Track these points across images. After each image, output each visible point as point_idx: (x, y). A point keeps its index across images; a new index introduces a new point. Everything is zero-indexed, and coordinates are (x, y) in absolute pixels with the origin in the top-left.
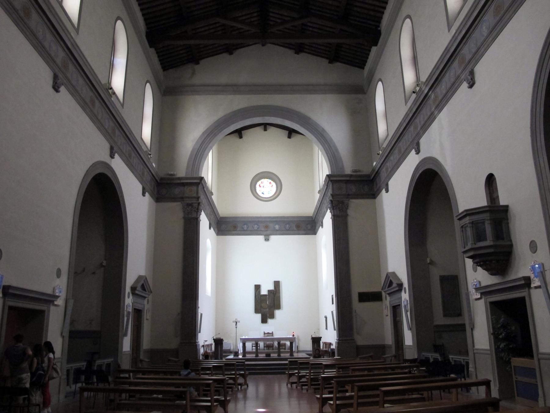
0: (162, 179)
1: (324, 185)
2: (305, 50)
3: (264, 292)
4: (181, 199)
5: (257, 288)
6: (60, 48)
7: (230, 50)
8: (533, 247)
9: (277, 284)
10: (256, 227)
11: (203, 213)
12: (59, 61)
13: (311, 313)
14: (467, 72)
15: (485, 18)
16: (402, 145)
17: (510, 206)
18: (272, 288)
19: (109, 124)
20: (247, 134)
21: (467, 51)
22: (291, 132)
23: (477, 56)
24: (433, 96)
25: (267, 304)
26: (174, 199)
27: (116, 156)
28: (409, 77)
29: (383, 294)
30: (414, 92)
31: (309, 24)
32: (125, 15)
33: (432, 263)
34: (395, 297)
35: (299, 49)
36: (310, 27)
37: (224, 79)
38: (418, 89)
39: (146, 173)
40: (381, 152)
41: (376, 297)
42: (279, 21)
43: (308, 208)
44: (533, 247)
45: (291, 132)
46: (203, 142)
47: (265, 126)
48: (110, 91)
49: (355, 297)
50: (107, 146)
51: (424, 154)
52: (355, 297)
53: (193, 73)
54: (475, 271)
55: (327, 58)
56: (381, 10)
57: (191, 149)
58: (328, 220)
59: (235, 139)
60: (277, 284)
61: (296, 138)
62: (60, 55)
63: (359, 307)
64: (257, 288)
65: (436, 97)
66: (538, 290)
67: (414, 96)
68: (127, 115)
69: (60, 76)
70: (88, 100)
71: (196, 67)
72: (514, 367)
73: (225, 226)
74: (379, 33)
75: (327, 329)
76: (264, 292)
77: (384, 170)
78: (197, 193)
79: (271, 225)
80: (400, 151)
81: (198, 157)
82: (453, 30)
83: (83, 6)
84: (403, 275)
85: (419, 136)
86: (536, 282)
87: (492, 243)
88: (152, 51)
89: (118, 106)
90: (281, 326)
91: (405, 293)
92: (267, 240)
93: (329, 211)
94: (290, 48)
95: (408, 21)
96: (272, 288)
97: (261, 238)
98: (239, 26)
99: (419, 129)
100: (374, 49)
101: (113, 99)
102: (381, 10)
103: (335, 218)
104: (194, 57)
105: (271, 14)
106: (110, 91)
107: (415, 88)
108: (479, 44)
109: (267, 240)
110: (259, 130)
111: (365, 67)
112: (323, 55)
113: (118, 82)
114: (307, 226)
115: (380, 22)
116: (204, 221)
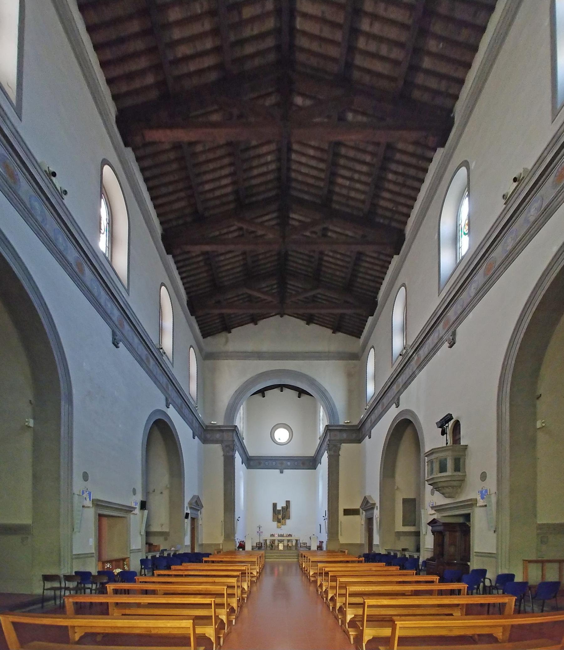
0: (207, 426)
1: (323, 434)
2: (315, 321)
3: (279, 508)
4: (220, 441)
5: (275, 505)
6: (114, 307)
7: (254, 320)
8: (483, 476)
9: (288, 502)
10: (274, 463)
11: (237, 452)
12: (115, 318)
13: (309, 521)
14: (450, 333)
15: (476, 278)
16: (385, 401)
17: (470, 446)
18: (284, 505)
19: (163, 380)
20: (268, 393)
21: (452, 314)
22: (301, 392)
23: (459, 319)
24: (416, 358)
25: (281, 514)
26: (216, 442)
27: (171, 406)
28: (398, 344)
29: (361, 510)
30: (401, 355)
31: (319, 296)
32: (168, 282)
33: (398, 488)
34: (370, 512)
35: (310, 320)
36: (320, 298)
37: (250, 347)
38: (405, 351)
39: (194, 421)
40: (368, 407)
41: (354, 512)
42: (294, 292)
43: (311, 453)
44: (483, 476)
45: (301, 392)
46: (236, 399)
47: (282, 387)
48: (161, 350)
49: (341, 512)
50: (163, 398)
51: (402, 407)
52: (341, 512)
53: (227, 341)
54: (432, 493)
55: (331, 328)
56: (380, 280)
57: (227, 404)
58: (325, 459)
59: (258, 397)
60: (288, 502)
61: (304, 397)
62: (116, 314)
63: (342, 518)
64: (275, 505)
65: (419, 358)
66: (482, 508)
67: (401, 357)
68: (176, 373)
69: (118, 333)
70: (144, 358)
71: (229, 335)
72: (28, 538)
73: (252, 462)
74: (376, 304)
75: (123, 615)
76: (279, 508)
77: (369, 420)
78: (233, 437)
79: (285, 462)
80: (383, 405)
81: (232, 411)
82: (443, 294)
83: (25, 64)
84: (376, 499)
85: (400, 392)
86: (481, 502)
87: (450, 474)
88: (170, 259)
89: (169, 365)
90: (290, 527)
91: (377, 509)
92: (282, 472)
93: (326, 452)
94: (303, 320)
95: (403, 288)
96: (284, 505)
97: (278, 471)
98: (263, 297)
99: (401, 386)
100: (396, 259)
101: (164, 358)
102: (380, 280)
103: (330, 457)
104: (227, 326)
105: (289, 286)
106: (161, 350)
107: (403, 350)
108: (465, 306)
109: (282, 472)
110: (277, 391)
111: (361, 337)
112: (328, 326)
113: (167, 343)
114: (311, 463)
115: (377, 293)
116: (238, 458)
